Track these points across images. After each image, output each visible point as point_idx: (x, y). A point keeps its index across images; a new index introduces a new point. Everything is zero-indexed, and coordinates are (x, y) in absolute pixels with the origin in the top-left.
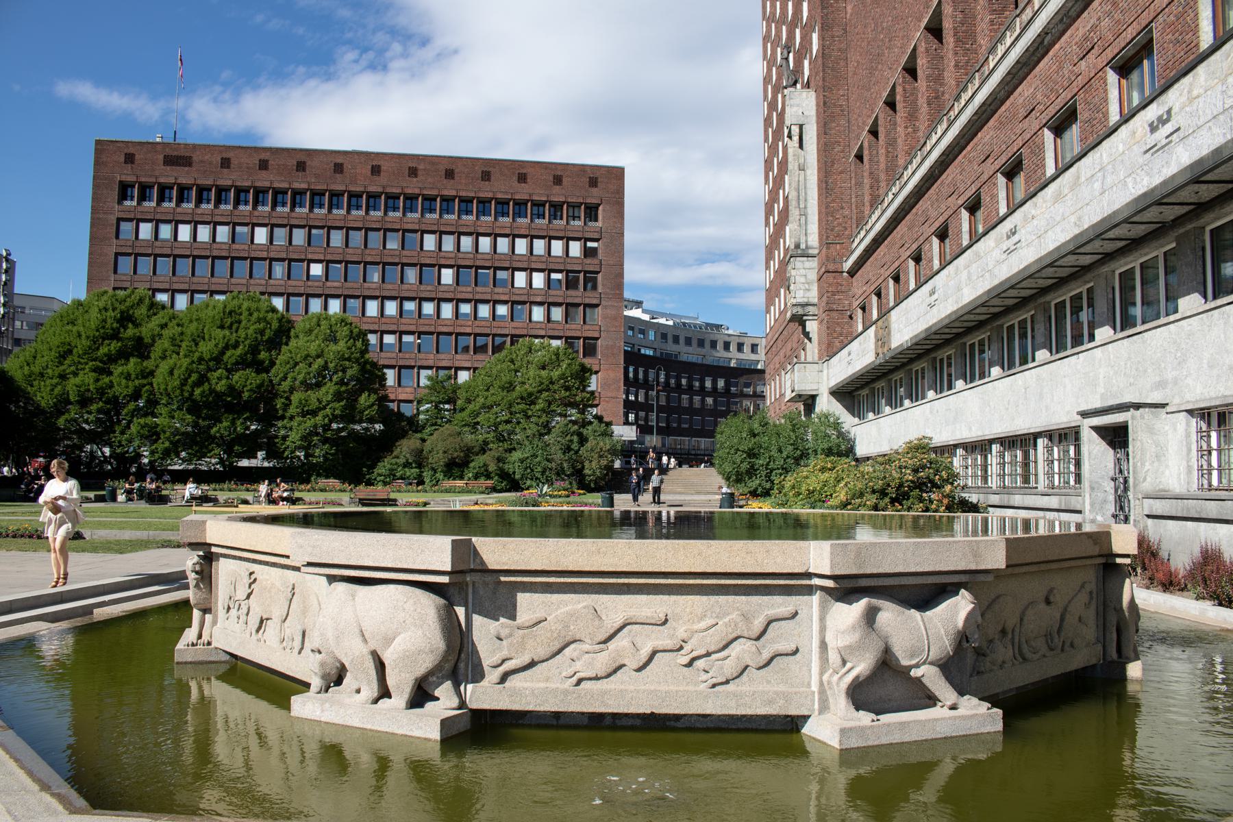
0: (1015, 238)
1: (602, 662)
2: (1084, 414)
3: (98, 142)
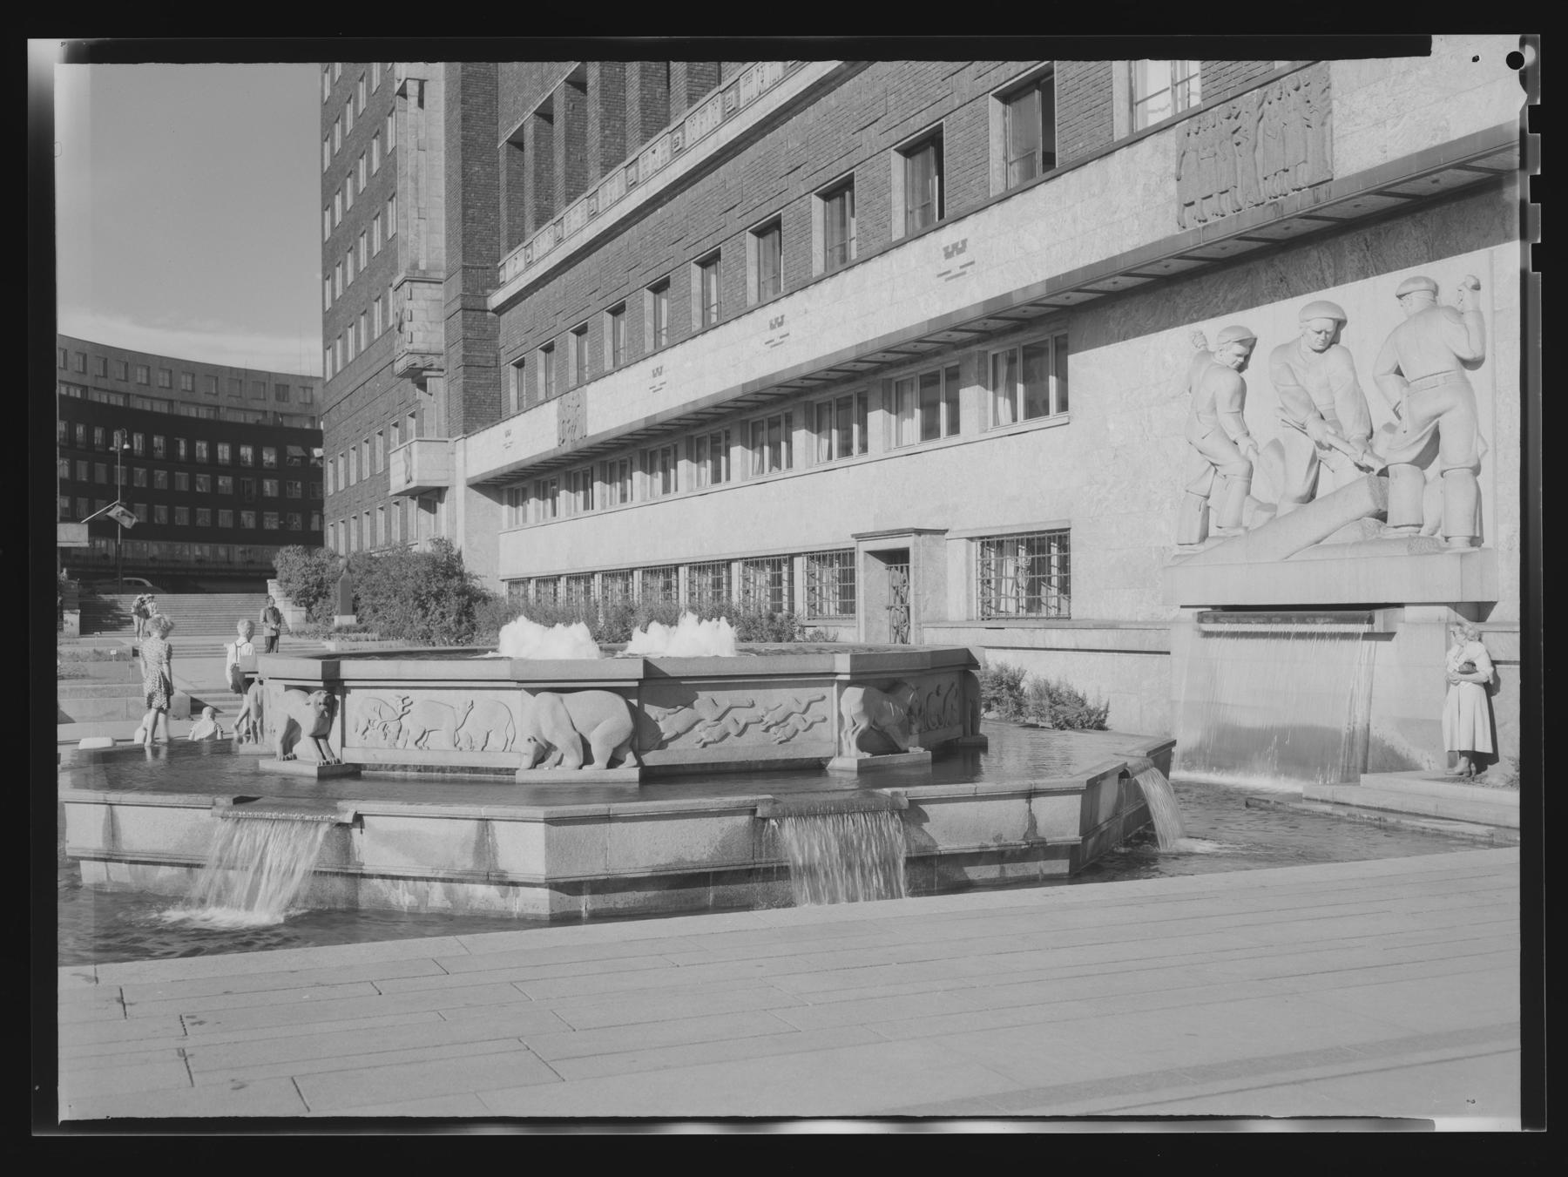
0: (782, 330)
1: (716, 733)
2: (860, 537)
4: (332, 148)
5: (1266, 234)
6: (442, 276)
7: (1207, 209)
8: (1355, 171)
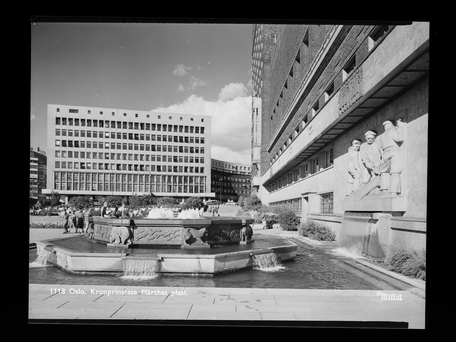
1: (152, 237)
2: (303, 195)
3: (56, 162)
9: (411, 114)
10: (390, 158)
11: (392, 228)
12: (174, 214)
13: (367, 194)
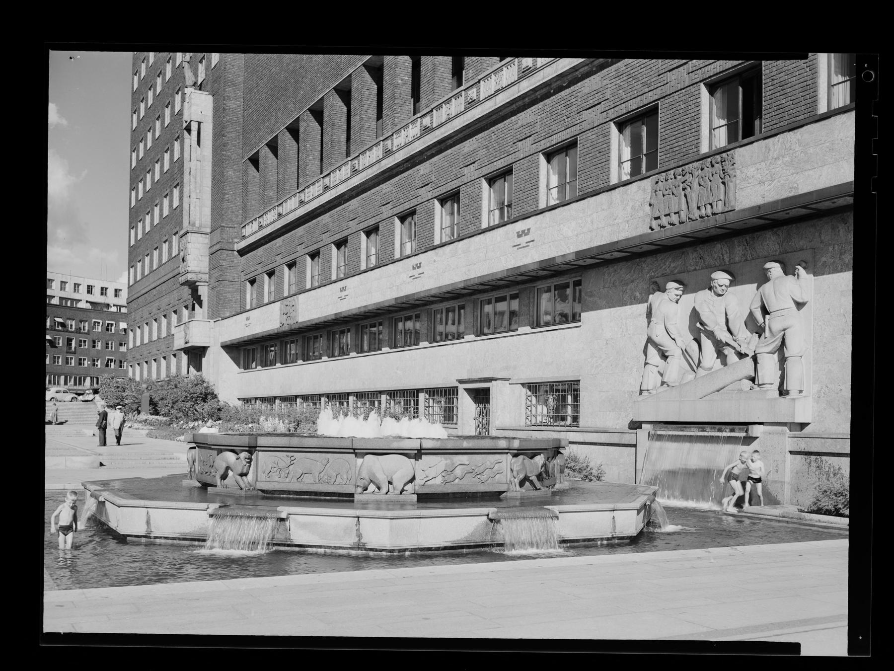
2: (461, 382)
4: (138, 156)
5: (696, 235)
6: (209, 230)
7: (664, 221)
8: (748, 206)
9: (823, 259)
10: (784, 330)
11: (791, 452)
12: (356, 415)
13: (718, 391)
